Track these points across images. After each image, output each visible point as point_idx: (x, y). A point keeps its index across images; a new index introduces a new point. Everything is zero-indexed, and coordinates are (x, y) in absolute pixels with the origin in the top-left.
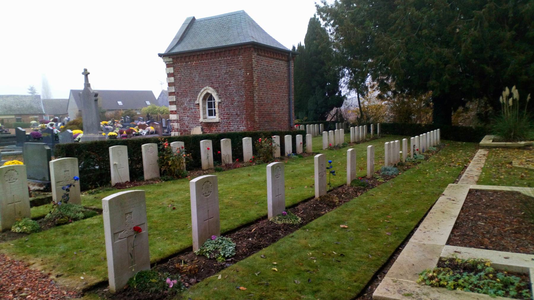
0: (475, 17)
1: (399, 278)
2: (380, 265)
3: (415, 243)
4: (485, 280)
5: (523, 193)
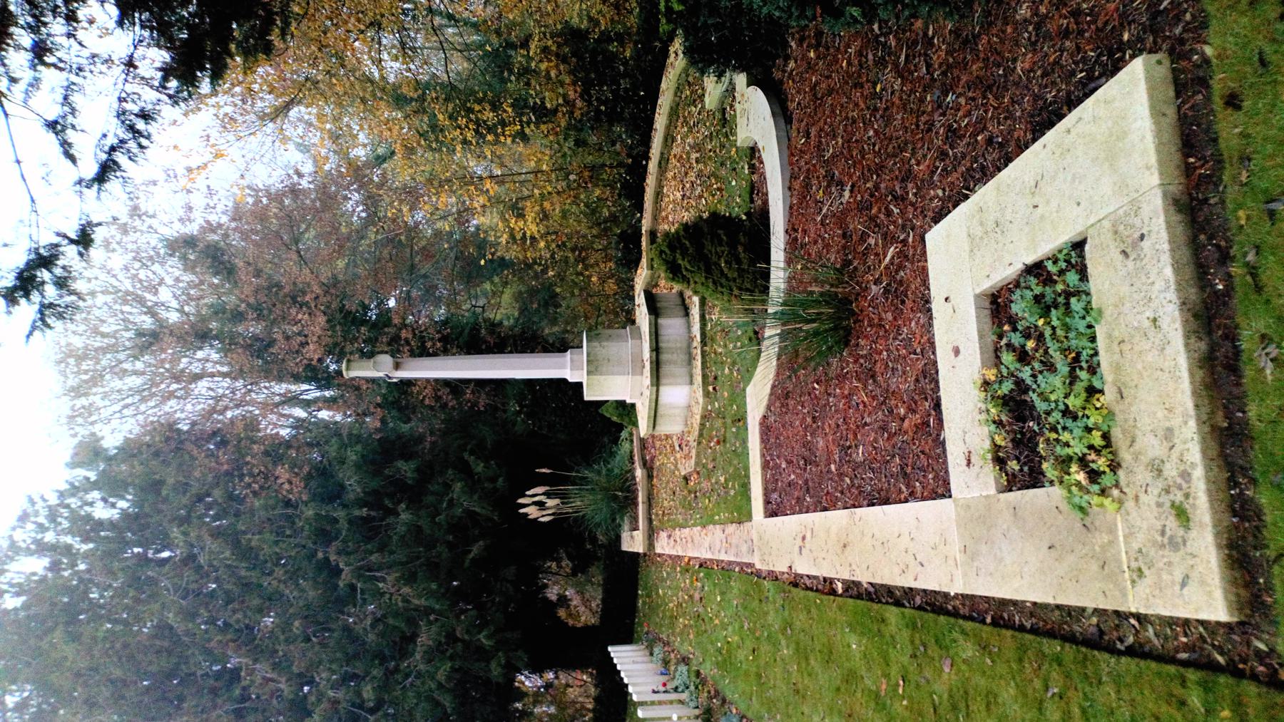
0: (354, 581)
1: (1120, 567)
2: (1078, 651)
3: (965, 575)
4: (1051, 351)
5: (772, 376)
